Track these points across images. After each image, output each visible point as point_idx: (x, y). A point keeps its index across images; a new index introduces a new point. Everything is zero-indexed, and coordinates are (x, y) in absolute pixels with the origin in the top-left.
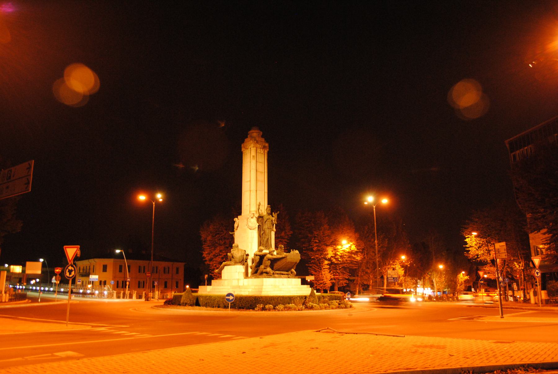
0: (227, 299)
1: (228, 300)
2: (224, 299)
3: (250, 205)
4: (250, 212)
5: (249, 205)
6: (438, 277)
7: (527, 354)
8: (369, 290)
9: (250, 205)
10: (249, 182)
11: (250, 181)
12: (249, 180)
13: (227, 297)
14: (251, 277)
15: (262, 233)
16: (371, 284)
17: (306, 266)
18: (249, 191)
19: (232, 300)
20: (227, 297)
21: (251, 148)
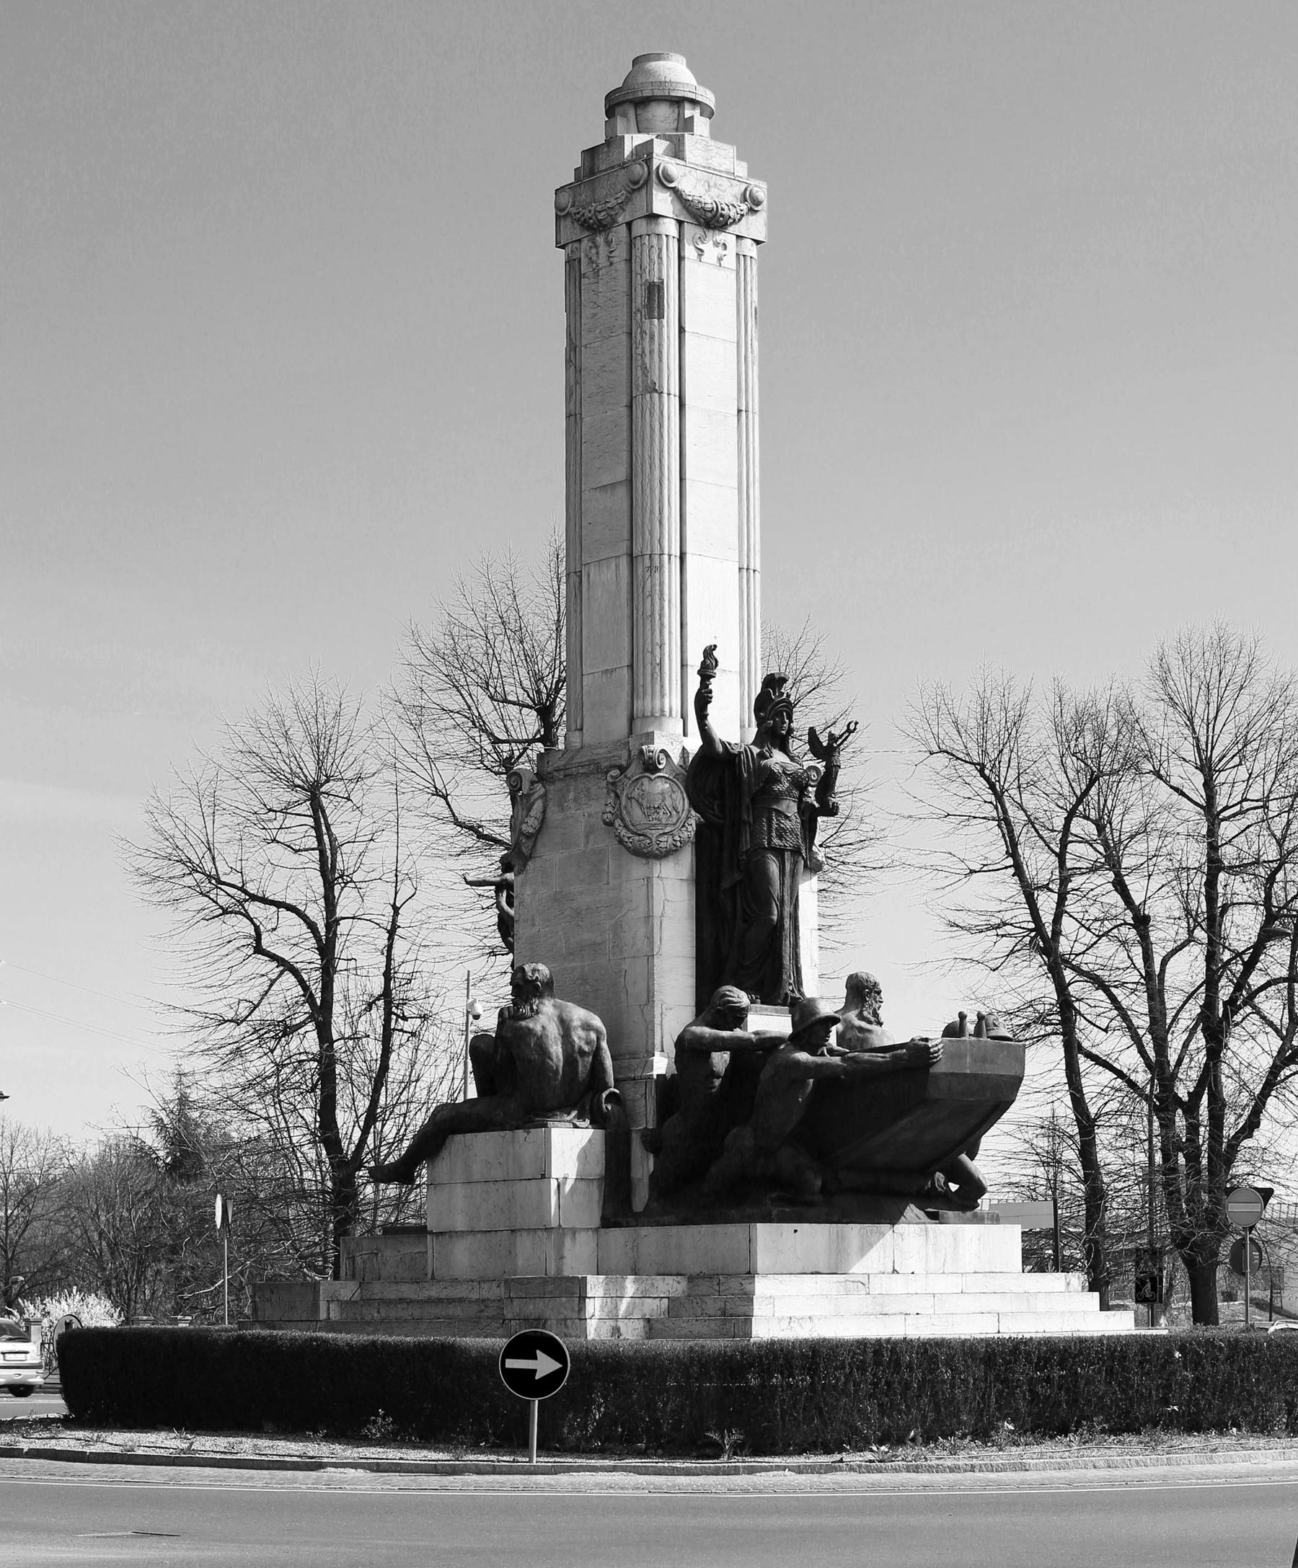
0: (512, 1375)
1: (524, 1380)
2: (494, 1374)
3: (631, 666)
4: (632, 719)
5: (625, 672)
6: (1260, 689)
7: (1218, 654)
8: (541, 1036)
9: (631, 666)
10: (622, 492)
11: (630, 482)
12: (621, 473)
13: (511, 1364)
14: (649, 1218)
15: (726, 884)
16: (579, 964)
17: (798, 1063)
18: (624, 562)
19: (555, 1377)
20: (511, 1364)
21: (629, 225)
